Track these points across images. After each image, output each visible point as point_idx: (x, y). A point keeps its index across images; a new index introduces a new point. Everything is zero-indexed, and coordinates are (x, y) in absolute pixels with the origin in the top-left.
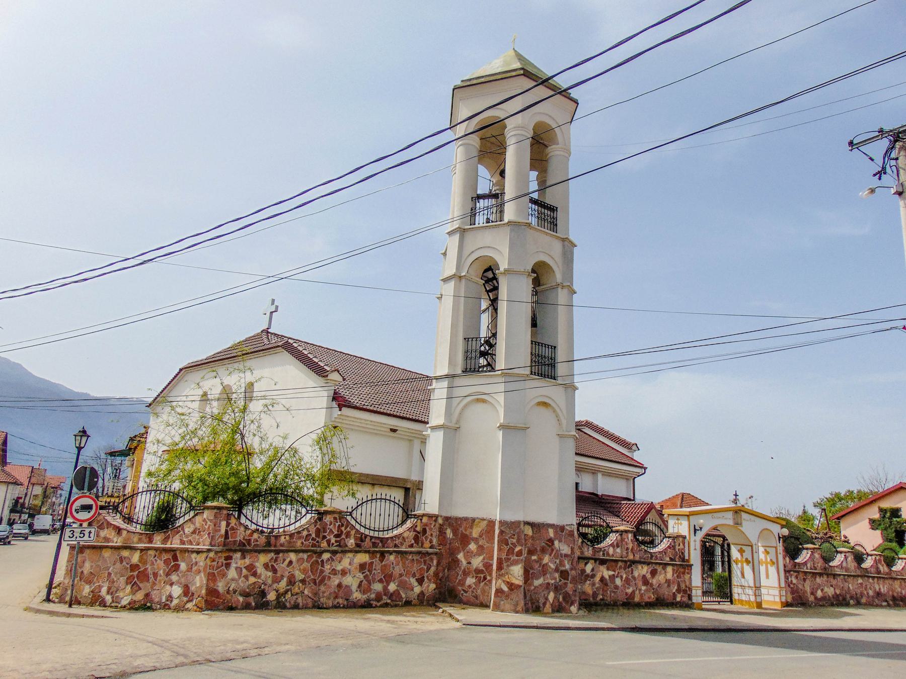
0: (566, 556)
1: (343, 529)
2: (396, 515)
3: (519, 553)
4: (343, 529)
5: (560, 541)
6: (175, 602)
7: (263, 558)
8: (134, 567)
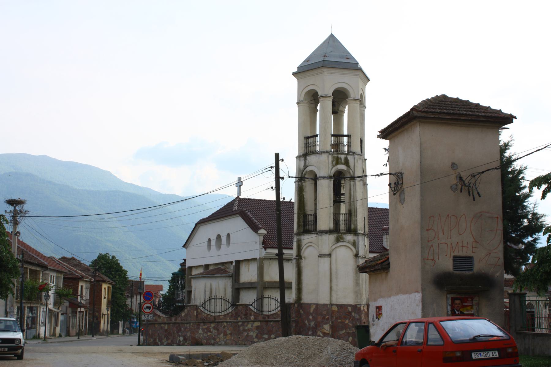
0: (358, 319)
3: (328, 319)
5: (355, 313)
6: (182, 343)
7: (213, 325)
8: (166, 331)
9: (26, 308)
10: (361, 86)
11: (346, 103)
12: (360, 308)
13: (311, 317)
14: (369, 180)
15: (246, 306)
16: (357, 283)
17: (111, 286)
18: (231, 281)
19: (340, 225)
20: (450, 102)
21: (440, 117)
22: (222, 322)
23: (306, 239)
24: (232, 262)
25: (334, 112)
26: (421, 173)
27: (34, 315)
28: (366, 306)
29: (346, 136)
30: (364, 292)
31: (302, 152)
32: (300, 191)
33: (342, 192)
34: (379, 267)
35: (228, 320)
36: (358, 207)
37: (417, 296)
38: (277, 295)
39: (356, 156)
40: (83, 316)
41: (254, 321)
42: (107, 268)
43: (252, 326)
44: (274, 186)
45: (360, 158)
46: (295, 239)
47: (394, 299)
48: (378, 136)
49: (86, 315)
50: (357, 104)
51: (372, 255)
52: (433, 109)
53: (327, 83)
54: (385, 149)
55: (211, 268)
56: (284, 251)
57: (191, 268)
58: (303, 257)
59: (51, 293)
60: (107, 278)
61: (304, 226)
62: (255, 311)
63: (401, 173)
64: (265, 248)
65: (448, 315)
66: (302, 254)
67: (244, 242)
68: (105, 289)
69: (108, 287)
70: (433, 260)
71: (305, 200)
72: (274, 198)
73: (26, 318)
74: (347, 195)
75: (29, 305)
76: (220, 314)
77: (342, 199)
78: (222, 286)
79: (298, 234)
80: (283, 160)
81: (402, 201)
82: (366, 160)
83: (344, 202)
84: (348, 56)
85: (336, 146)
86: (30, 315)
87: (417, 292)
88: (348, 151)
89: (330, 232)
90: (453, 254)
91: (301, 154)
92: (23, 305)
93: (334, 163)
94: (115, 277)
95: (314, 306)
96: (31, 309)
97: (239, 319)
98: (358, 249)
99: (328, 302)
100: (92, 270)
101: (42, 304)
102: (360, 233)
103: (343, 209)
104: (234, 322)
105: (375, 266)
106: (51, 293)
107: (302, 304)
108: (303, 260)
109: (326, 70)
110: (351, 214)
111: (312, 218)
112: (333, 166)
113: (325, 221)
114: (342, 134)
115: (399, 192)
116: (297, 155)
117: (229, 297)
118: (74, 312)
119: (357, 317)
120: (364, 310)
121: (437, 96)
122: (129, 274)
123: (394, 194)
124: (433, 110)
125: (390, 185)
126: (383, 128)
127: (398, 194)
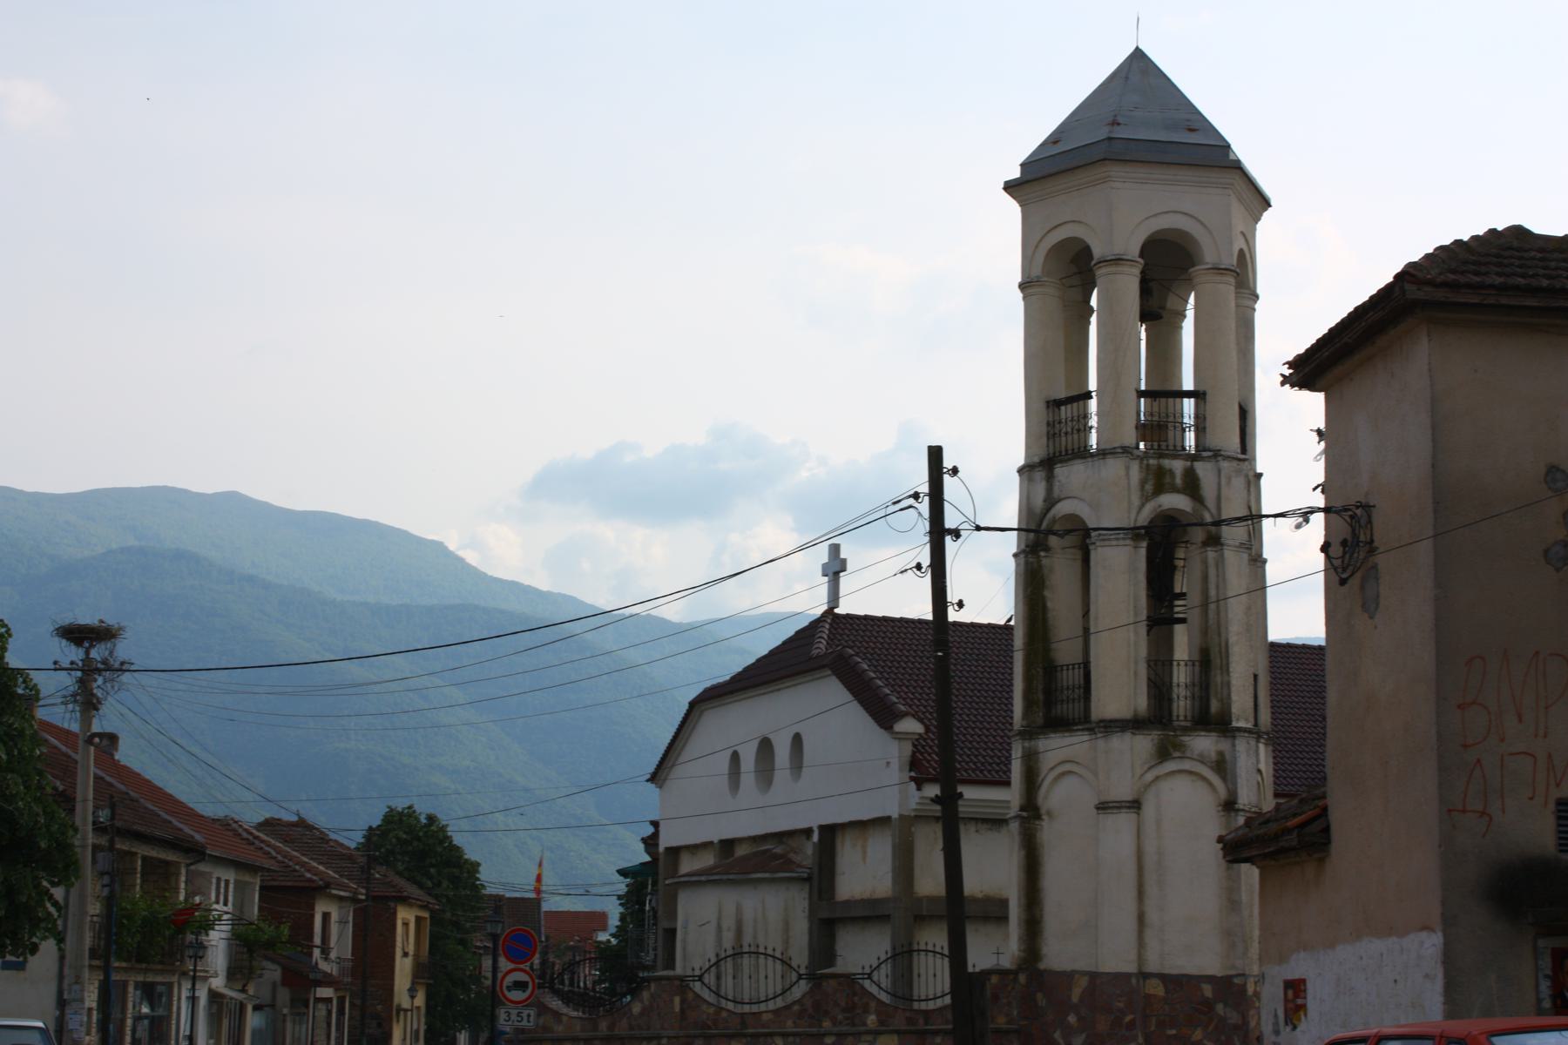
9: (131, 989)
10: (1239, 225)
11: (1190, 285)
12: (1243, 987)
13: (1072, 1019)
15: (849, 980)
16: (1232, 902)
17: (426, 915)
19: (1170, 700)
20: (1541, 250)
21: (1504, 301)
23: (1056, 748)
27: (160, 1012)
29: (1189, 394)
31: (1040, 453)
33: (1177, 590)
35: (789, 1026)
36: (1233, 639)
38: (935, 937)
39: (1225, 464)
40: (329, 1012)
41: (877, 1033)
42: (415, 852)
44: (926, 561)
45: (1239, 472)
46: (1017, 752)
48: (1286, 380)
49: (341, 1012)
50: (1227, 288)
52: (1477, 274)
53: (1125, 215)
54: (1319, 432)
55: (741, 851)
56: (970, 793)
57: (675, 852)
58: (1043, 811)
59: (217, 938)
60: (412, 890)
61: (1049, 702)
63: (1367, 507)
65: (1540, 1012)
67: (851, 765)
68: (406, 924)
69: (418, 919)
70: (1483, 813)
71: (1050, 615)
72: (922, 609)
73: (129, 1022)
74: (1194, 598)
75: (140, 978)
76: (763, 1007)
78: (775, 913)
79: (1029, 733)
80: (955, 471)
81: (1370, 606)
82: (1260, 475)
83: (1183, 621)
84: (1195, 121)
86: (145, 1010)
89: (1135, 724)
90: (1556, 794)
91: (1036, 460)
92: (115, 977)
93: (1149, 487)
94: (439, 884)
95: (1084, 982)
96: (149, 992)
97: (827, 1024)
98: (1235, 784)
99: (1131, 968)
100: (362, 860)
101: (184, 974)
102: (1239, 729)
103: (1183, 644)
104: (812, 1035)
106: (217, 938)
107: (1041, 973)
108: (1045, 823)
109: (1116, 171)
110: (1209, 661)
111: (1074, 677)
112: (1145, 499)
113: (1118, 687)
114: (1175, 388)
115: (1358, 575)
116: (1021, 462)
118: (300, 1003)
119: (1234, 1018)
121: (1493, 232)
122: (484, 875)
123: (1343, 582)
124: (1478, 279)
125: (1325, 548)
127: (1355, 582)
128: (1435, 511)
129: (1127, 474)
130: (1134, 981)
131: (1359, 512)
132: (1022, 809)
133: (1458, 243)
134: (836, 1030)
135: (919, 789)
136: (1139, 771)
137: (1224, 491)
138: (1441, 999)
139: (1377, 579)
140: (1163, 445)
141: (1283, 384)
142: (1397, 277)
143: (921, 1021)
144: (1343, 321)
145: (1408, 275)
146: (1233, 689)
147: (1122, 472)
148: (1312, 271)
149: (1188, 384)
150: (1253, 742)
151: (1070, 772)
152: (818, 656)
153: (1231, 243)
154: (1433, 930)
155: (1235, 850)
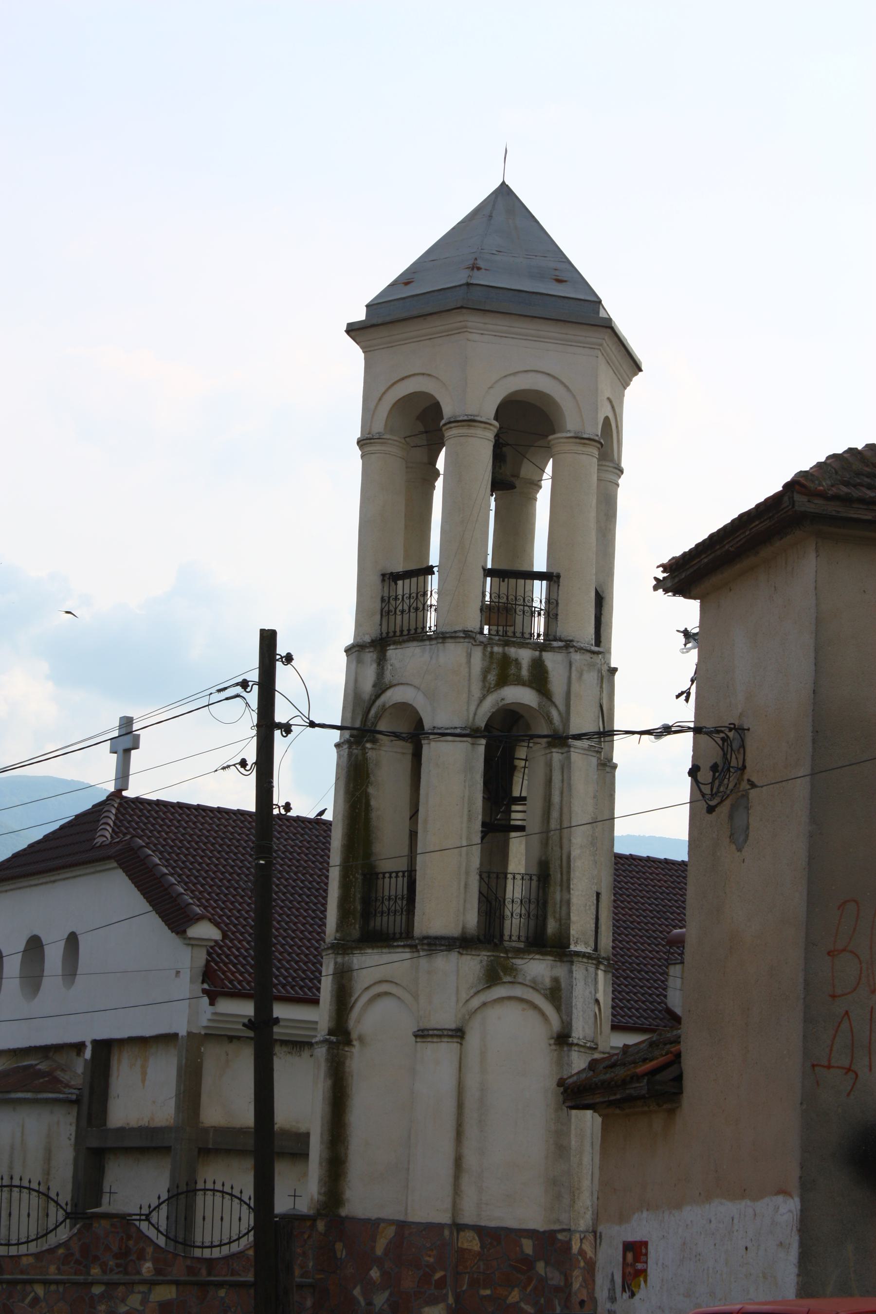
0: (557, 1289)
1: (131, 1243)
2: (24, 1213)
4: (131, 1243)
5: (547, 1263)
10: (606, 390)
11: (548, 451)
12: (568, 1245)
13: (375, 1273)
14: (623, 750)
15: (124, 1221)
16: (560, 1148)
18: (72, 1118)
19: (502, 918)
22: (25, 1282)
23: (372, 966)
24: (79, 1047)
25: (500, 484)
26: (816, 732)
28: (591, 1237)
29: (540, 576)
30: (586, 1183)
31: (372, 632)
32: (355, 778)
33: (516, 793)
34: (642, 1088)
35: (52, 1272)
36: (575, 853)
37: (782, 1210)
38: (241, 1178)
39: (577, 657)
41: (152, 1284)
43: (144, 1302)
44: (251, 757)
45: (591, 666)
46: (328, 967)
47: (692, 1214)
48: (659, 584)
50: (589, 460)
51: (620, 1040)
53: (481, 371)
54: (686, 634)
56: (280, 1011)
58: (354, 1035)
61: (367, 914)
62: (161, 1241)
63: (740, 730)
64: (213, 997)
66: (351, 1024)
67: (133, 972)
70: (849, 1070)
71: (373, 815)
74: (535, 804)
76: (23, 1249)
77: (517, 818)
79: (343, 947)
80: (289, 659)
81: (739, 837)
82: (615, 670)
83: (521, 828)
84: (564, 271)
85: (504, 613)
87: (783, 1192)
88: (546, 634)
89: (462, 943)
91: (368, 639)
93: (492, 678)
95: (391, 1231)
97: (96, 1271)
98: (570, 1014)
99: (444, 1218)
102: (578, 954)
103: (519, 856)
105: (624, 1083)
109: (474, 321)
110: (547, 876)
111: (394, 887)
112: (487, 691)
113: (446, 901)
114: (525, 568)
115: (727, 803)
116: (349, 640)
117: (62, 1184)
119: (555, 1278)
120: (582, 1252)
123: (711, 810)
125: (693, 772)
126: (678, 553)
128: (814, 741)
129: (469, 662)
130: (447, 1233)
131: (731, 734)
132: (330, 1033)
133: (851, 451)
134: (106, 1278)
135: (212, 1003)
136: (464, 996)
137: (575, 687)
138: (795, 1270)
139: (747, 808)
140: (510, 630)
141: (656, 588)
142: (788, 486)
143: (204, 1272)
144: (725, 527)
145: (796, 486)
146: (573, 909)
147: (463, 660)
148: (689, 462)
149: (540, 564)
150: (592, 969)
151: (387, 994)
152: (102, 846)
153: (596, 410)
154: (791, 1196)
155: (574, 1094)
